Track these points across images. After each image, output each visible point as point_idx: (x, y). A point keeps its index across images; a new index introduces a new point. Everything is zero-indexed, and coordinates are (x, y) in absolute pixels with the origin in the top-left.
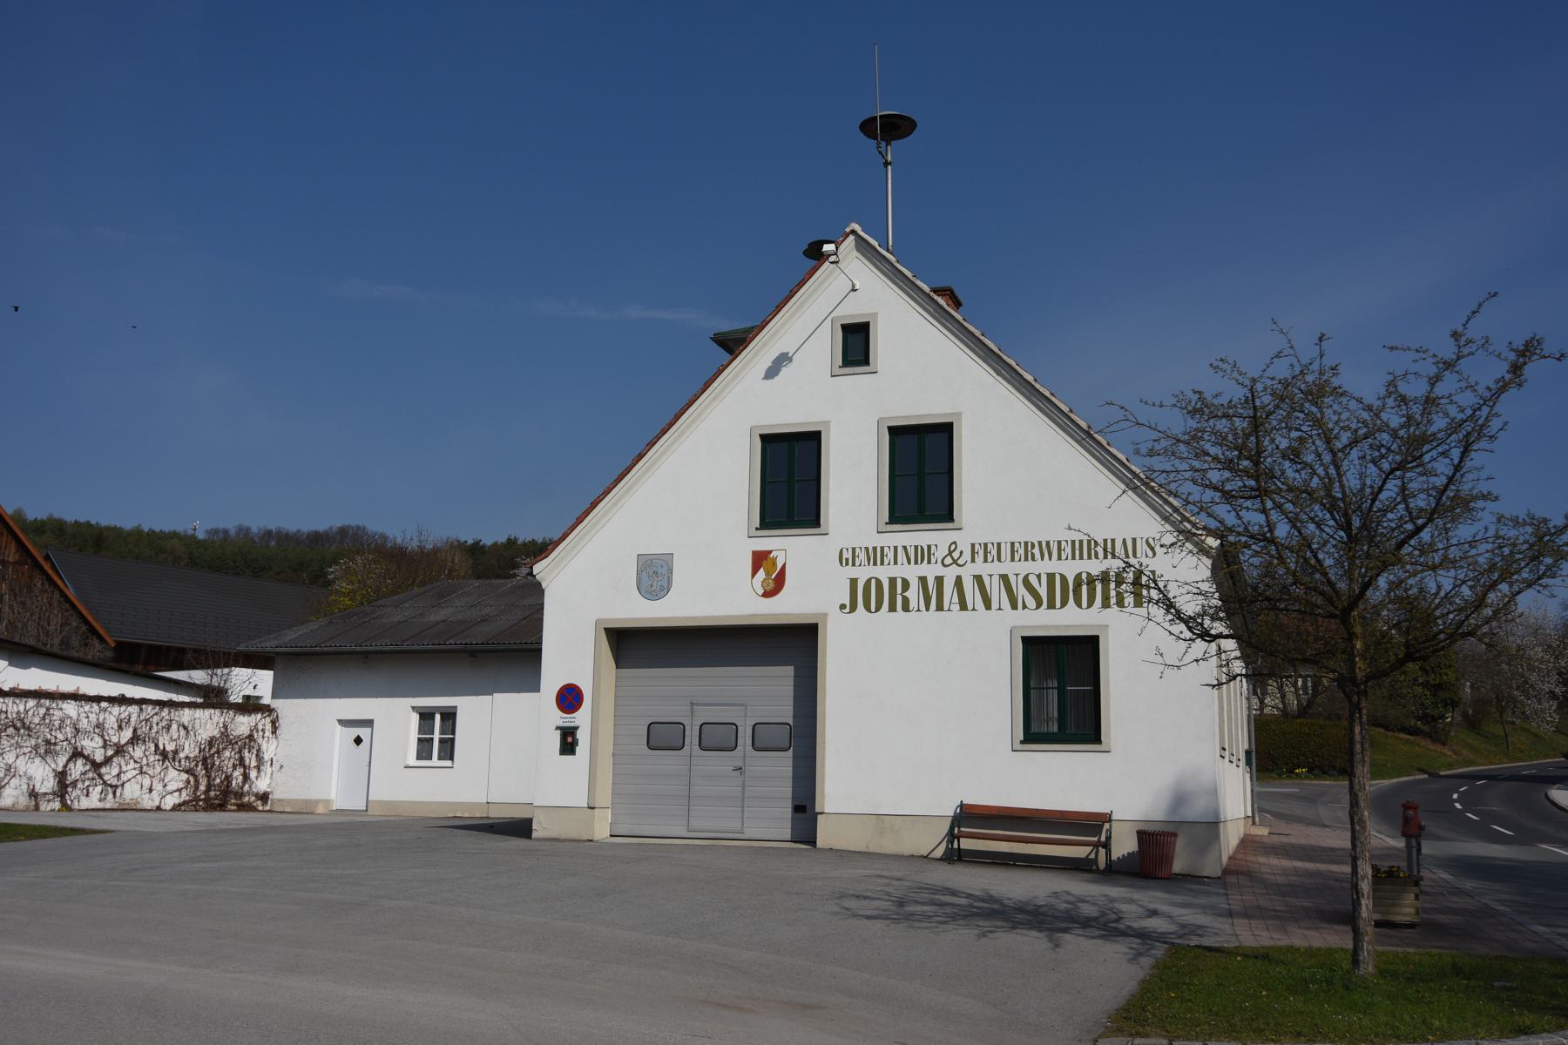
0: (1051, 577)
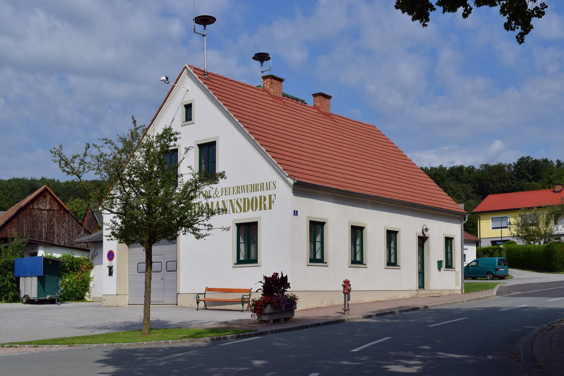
0: (244, 199)
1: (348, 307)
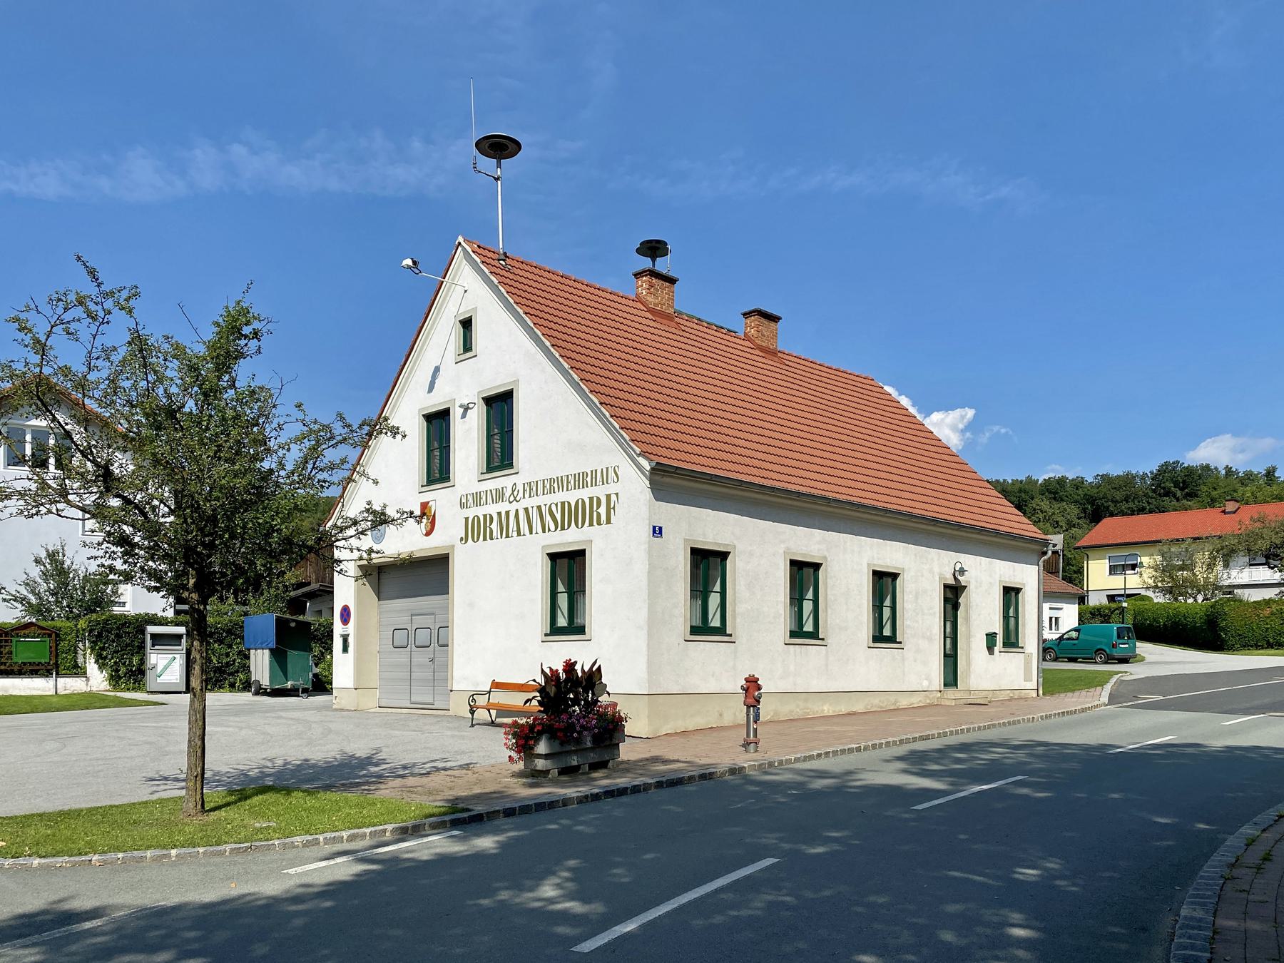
0: (563, 503)
1: (755, 735)
